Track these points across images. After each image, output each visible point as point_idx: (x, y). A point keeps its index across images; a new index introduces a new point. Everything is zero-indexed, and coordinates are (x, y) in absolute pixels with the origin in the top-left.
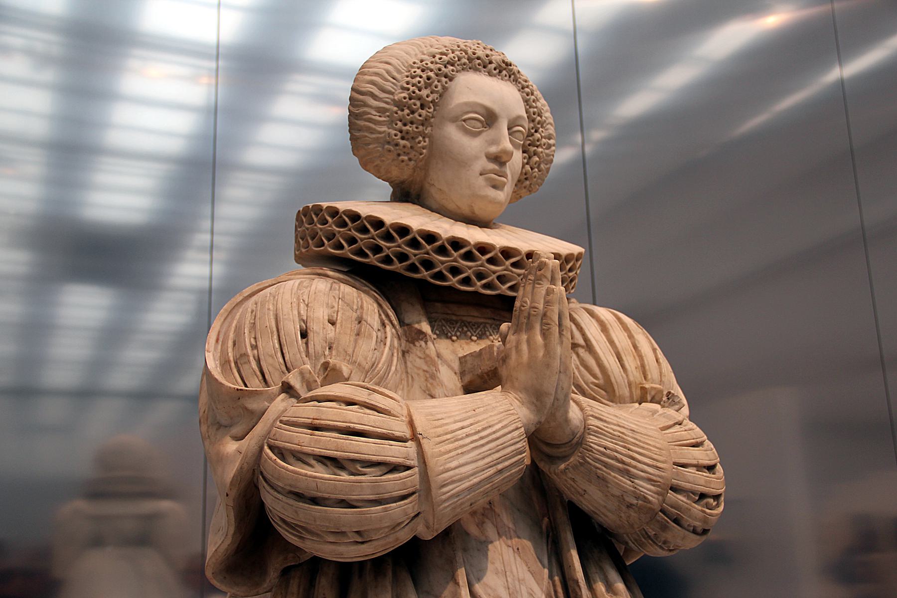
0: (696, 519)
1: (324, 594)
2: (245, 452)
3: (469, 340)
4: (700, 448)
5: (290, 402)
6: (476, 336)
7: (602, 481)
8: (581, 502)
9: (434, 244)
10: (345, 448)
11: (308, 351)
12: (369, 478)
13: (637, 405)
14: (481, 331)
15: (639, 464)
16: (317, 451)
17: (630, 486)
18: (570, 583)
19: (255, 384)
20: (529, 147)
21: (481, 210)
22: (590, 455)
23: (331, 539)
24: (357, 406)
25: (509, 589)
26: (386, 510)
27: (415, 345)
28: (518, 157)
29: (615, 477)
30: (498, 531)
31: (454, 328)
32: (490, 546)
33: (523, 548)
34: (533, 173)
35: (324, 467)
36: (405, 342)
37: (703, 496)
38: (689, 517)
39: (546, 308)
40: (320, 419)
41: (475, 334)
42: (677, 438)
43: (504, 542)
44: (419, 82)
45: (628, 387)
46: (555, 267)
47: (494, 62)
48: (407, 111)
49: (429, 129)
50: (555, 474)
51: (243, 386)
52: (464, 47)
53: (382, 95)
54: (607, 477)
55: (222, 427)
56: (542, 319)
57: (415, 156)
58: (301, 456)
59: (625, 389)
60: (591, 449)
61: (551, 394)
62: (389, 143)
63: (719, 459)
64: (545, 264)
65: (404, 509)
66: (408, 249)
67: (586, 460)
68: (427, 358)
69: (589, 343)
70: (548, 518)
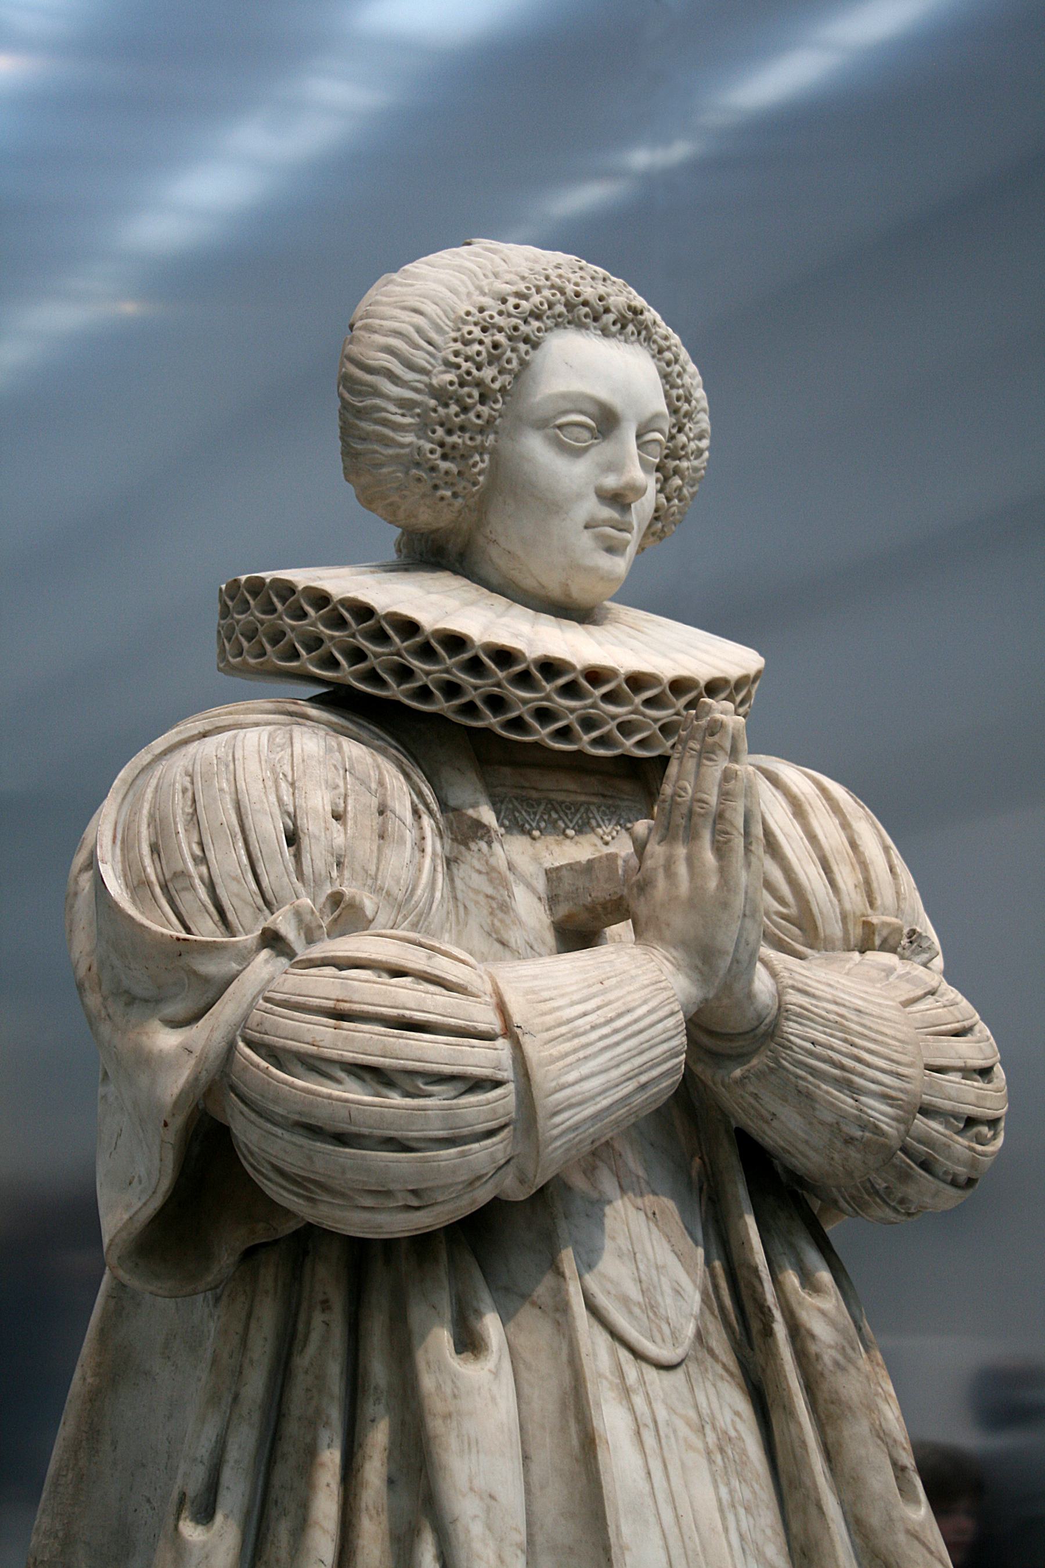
0: (958, 1162)
1: (325, 1293)
2: (202, 1050)
3: (561, 837)
4: (969, 1037)
5: (279, 964)
6: (573, 828)
7: (806, 1097)
8: (764, 1132)
9: (511, 670)
10: (398, 1052)
11: (302, 871)
12: (438, 1102)
13: (856, 955)
14: (581, 818)
15: (867, 1069)
16: (349, 1056)
17: (852, 1107)
18: (742, 1273)
19: (207, 930)
20: (666, 461)
21: (581, 591)
22: (788, 1055)
23: (368, 1202)
24: (409, 979)
25: (640, 1282)
26: (463, 1154)
27: (469, 849)
28: (650, 482)
29: (827, 1092)
30: (619, 1183)
31: (535, 814)
32: (608, 1210)
33: (662, 1212)
34: (670, 507)
35: (359, 1083)
36: (450, 841)
37: (971, 1122)
38: (948, 1158)
39: (723, 804)
40: (351, 1002)
41: (571, 826)
42: (931, 1020)
43: (630, 1201)
44: (479, 354)
45: (840, 922)
46: (739, 730)
47: (613, 309)
48: (454, 408)
49: (492, 437)
50: (724, 1086)
51: (184, 932)
52: (558, 280)
53: (409, 376)
54: (815, 1092)
55: (137, 1001)
56: (714, 822)
57: (464, 488)
58: (317, 1063)
59: (836, 925)
60: (789, 1044)
61: (726, 953)
62: (418, 465)
63: (999, 1055)
64: (722, 725)
65: (492, 1153)
66: (463, 676)
67: (780, 1062)
68: (491, 873)
69: (771, 839)
70: (700, 1158)
